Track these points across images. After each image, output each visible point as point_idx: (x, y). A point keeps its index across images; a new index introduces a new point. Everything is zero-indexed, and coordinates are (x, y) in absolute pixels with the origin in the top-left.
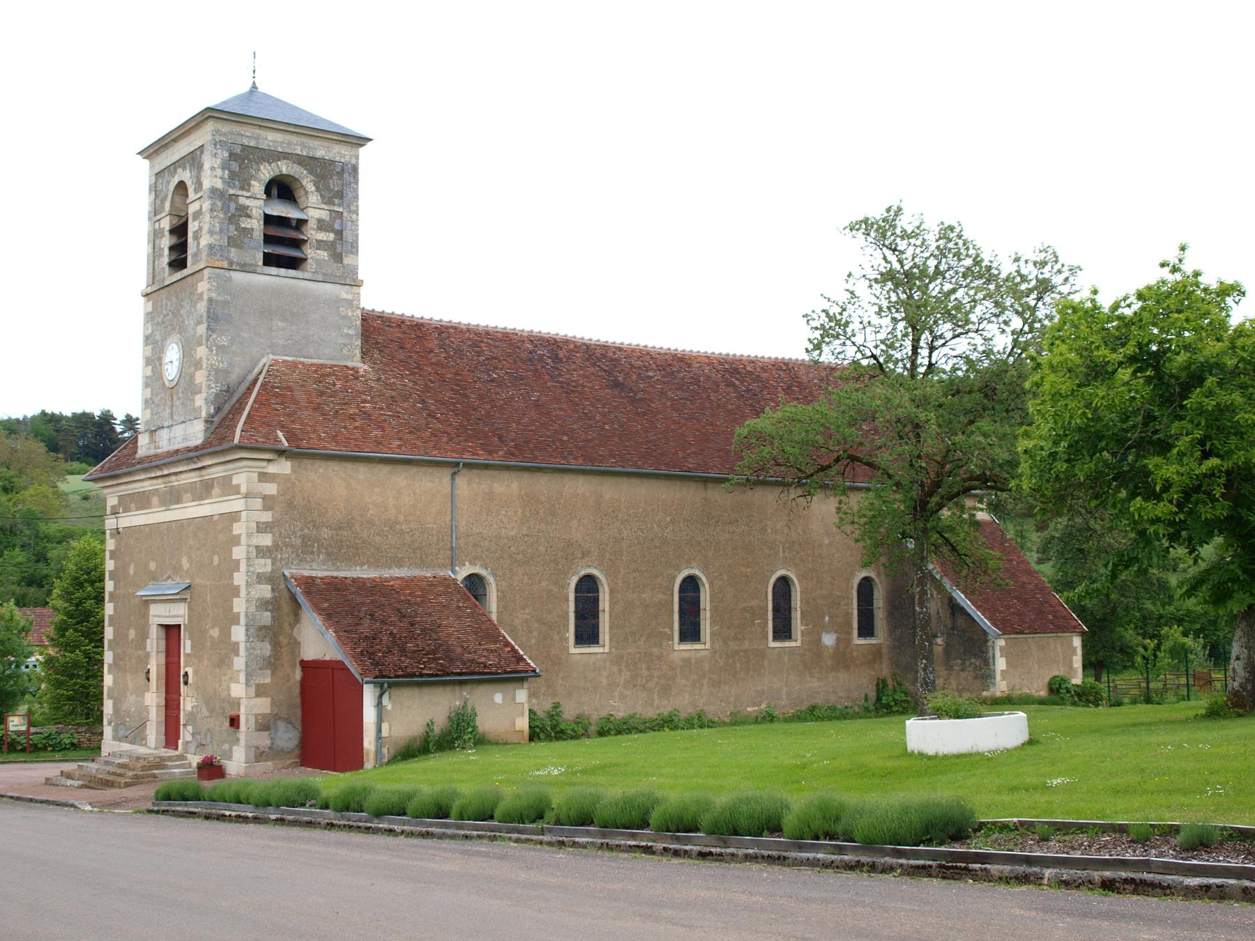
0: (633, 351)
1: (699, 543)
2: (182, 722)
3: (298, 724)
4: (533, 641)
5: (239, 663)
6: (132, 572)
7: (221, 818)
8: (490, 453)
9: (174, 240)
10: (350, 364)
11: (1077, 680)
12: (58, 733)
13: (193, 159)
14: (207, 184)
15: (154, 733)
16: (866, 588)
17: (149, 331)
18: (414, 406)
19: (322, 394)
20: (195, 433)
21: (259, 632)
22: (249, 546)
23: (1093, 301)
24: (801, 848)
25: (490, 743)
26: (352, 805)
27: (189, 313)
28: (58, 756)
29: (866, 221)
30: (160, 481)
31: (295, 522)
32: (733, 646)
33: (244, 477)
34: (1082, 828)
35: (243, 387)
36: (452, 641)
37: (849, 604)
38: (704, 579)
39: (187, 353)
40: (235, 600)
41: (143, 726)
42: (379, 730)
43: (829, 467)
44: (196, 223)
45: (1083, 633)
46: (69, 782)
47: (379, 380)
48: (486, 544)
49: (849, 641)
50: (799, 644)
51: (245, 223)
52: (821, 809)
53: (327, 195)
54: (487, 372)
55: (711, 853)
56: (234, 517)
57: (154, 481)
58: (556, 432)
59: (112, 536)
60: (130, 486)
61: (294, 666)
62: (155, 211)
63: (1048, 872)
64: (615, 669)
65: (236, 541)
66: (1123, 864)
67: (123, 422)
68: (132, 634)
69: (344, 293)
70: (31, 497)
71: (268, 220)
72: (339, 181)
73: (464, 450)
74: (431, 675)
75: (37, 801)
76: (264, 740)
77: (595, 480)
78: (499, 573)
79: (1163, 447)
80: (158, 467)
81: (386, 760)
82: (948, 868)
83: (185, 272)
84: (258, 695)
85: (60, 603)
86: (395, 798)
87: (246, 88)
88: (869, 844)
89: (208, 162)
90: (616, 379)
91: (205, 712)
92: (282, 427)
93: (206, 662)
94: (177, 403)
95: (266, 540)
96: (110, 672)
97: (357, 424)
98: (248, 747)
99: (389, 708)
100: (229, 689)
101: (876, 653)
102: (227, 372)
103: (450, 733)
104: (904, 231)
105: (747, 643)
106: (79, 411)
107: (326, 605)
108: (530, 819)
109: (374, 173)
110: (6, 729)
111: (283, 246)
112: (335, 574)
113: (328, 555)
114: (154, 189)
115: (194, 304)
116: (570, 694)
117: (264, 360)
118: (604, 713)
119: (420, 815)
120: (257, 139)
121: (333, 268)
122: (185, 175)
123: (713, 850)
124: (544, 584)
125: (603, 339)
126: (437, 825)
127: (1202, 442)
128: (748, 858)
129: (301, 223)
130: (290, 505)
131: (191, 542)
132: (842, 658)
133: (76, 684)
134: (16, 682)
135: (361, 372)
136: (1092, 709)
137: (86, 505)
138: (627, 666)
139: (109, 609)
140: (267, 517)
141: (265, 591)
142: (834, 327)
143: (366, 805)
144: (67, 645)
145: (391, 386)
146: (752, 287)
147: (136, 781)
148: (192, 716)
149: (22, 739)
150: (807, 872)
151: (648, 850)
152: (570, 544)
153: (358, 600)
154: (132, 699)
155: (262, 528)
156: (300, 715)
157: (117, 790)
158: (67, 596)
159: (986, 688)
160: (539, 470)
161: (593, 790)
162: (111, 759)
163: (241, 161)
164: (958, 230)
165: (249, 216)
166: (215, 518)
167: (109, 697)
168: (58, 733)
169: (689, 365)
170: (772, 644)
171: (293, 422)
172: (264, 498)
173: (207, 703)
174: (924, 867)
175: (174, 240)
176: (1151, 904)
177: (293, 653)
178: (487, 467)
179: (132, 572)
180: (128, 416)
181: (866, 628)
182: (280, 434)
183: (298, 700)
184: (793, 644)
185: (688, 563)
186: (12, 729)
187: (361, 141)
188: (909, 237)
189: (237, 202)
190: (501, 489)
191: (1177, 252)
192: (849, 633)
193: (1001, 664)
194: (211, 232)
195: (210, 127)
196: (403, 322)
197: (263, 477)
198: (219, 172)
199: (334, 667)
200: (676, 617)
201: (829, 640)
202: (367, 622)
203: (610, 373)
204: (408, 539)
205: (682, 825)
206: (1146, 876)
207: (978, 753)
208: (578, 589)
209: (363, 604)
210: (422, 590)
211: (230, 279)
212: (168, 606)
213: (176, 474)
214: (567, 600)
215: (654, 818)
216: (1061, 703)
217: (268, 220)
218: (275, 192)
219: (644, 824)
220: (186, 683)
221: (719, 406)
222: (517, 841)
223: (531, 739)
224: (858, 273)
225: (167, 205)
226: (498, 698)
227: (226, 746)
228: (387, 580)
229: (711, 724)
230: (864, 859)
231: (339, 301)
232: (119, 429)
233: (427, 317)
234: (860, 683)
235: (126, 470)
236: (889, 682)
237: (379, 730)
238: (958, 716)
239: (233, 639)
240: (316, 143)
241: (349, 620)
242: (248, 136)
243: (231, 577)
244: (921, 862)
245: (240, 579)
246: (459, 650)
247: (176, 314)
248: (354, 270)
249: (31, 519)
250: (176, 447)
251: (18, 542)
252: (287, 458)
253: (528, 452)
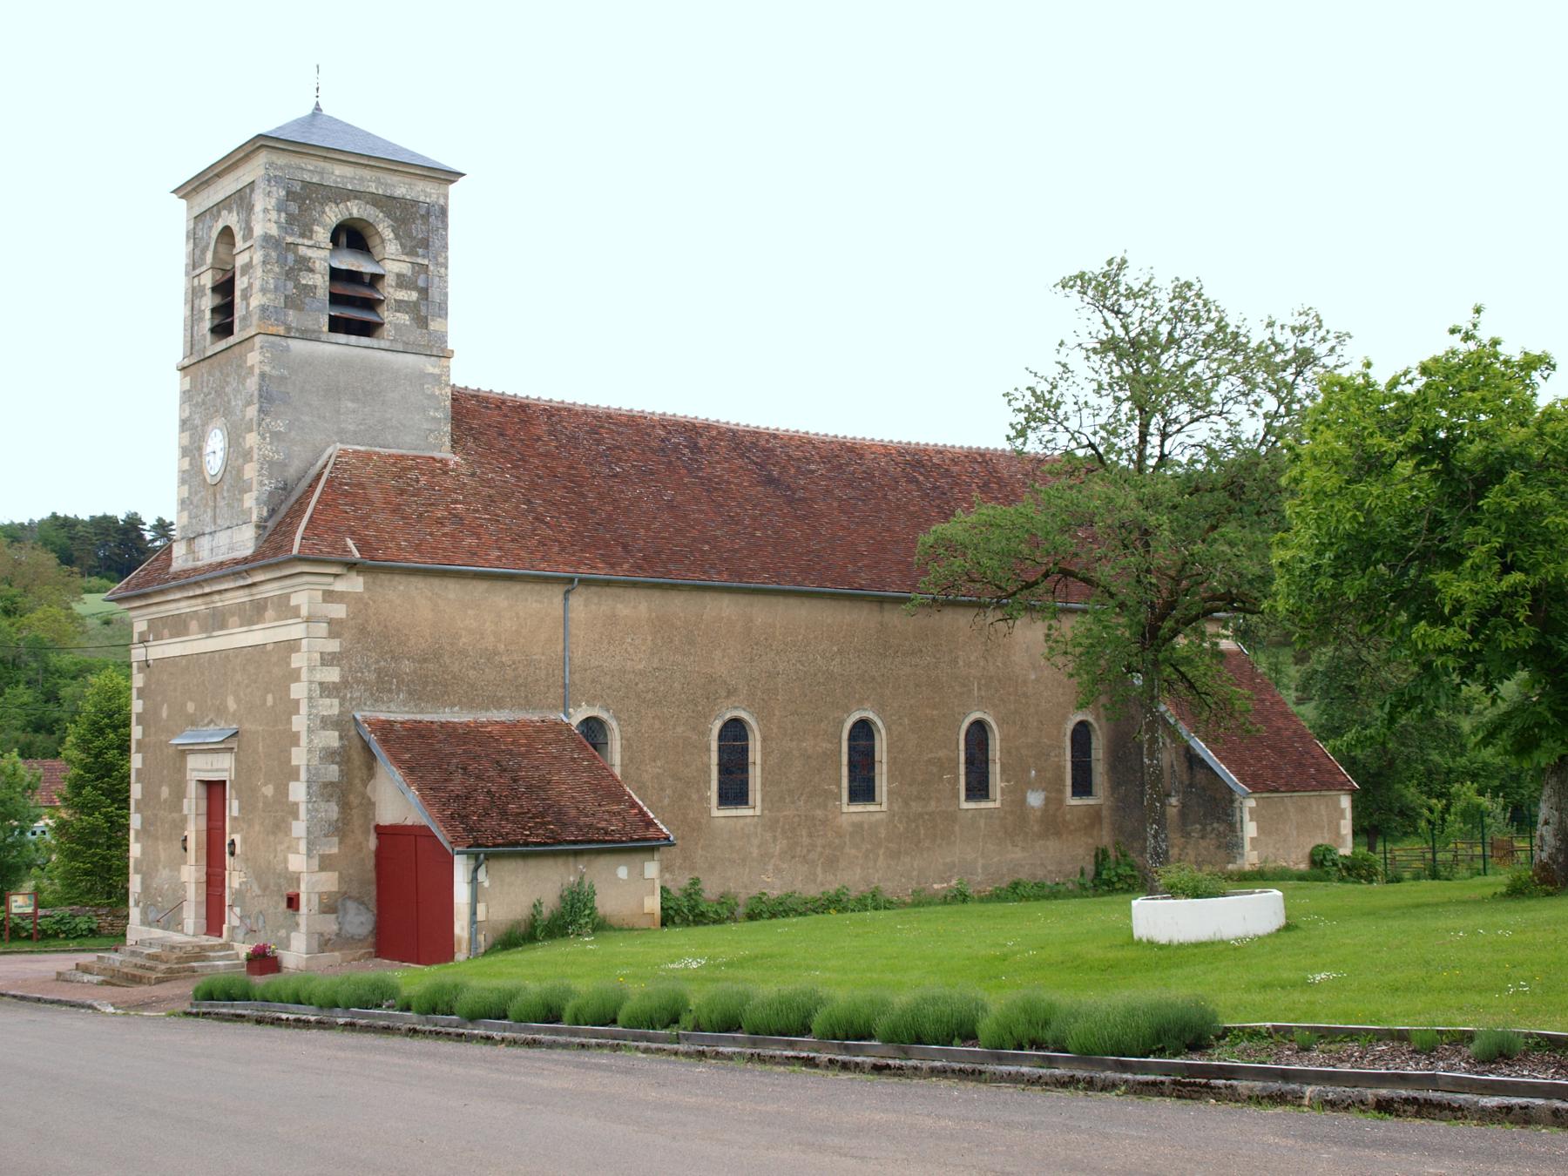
0: (791, 438)
1: (873, 679)
2: (227, 902)
3: (373, 905)
4: (666, 801)
5: (299, 828)
6: (164, 715)
7: (276, 1022)
8: (612, 566)
9: (218, 300)
10: (437, 455)
11: (1346, 850)
12: (73, 916)
13: (241, 198)
14: (258, 230)
15: (192, 916)
16: (1082, 734)
17: (187, 414)
18: (517, 507)
19: (402, 492)
20: (244, 541)
21: (324, 790)
22: (311, 682)
23: (1365, 376)
24: (1000, 1059)
25: (612, 928)
26: (440, 1007)
27: (236, 391)
28: (72, 945)
29: (1082, 276)
30: (200, 601)
31: (369, 652)
32: (916, 807)
33: (304, 596)
34: (1352, 1035)
35: (304, 484)
36: (565, 801)
37: (1061, 755)
38: (879, 723)
39: (234, 441)
40: (294, 750)
41: (179, 907)
42: (474, 913)
43: (1036, 583)
44: (245, 279)
45: (1353, 792)
46: (87, 978)
47: (473, 475)
48: (608, 679)
49: (1061, 801)
50: (998, 804)
51: (306, 279)
52: (1026, 1011)
53: (409, 244)
54: (608, 464)
55: (888, 1067)
56: (292, 646)
57: (193, 602)
58: (694, 540)
59: (140, 670)
60: (163, 608)
61: (367, 832)
62: (194, 264)
63: (1309, 1090)
64: (768, 836)
65: (295, 676)
66: (1404, 1079)
67: (154, 528)
68: (165, 792)
69: (430, 366)
70: (38, 621)
71: (335, 274)
72: (423, 226)
73: (580, 563)
74: (539, 844)
75: (46, 1001)
76: (330, 925)
77: (744, 600)
78: (624, 716)
79: (1453, 559)
80: (198, 584)
81: (482, 950)
82: (1185, 1085)
83: (231, 340)
84: (322, 868)
85: (75, 754)
86: (493, 998)
87: (308, 110)
88: (1086, 1055)
89: (260, 202)
90: (770, 474)
91: (256, 890)
92: (352, 534)
93: (257, 828)
94: (221, 503)
95: (333, 675)
96: (137, 840)
97: (446, 530)
98: (310, 934)
99: (486, 884)
100: (286, 861)
101: (1095, 816)
102: (283, 465)
103: (562, 916)
104: (1129, 288)
105: (933, 803)
106: (99, 514)
107: (407, 756)
108: (663, 1024)
109: (467, 216)
110: (8, 911)
111: (354, 307)
112: (419, 717)
113: (410, 693)
114: (193, 236)
115: (242, 380)
116: (712, 868)
117: (329, 451)
118: (755, 892)
119: (525, 1018)
120: (321, 173)
121: (416, 335)
122: (231, 219)
123: (890, 1062)
124: (679, 730)
126: (546, 1031)
127: (1501, 553)
128: (934, 1072)
129: (376, 279)
130: (363, 631)
131: (238, 677)
132: (1052, 823)
133: (94, 855)
134: (20, 853)
135: (451, 465)
136: (1364, 886)
137: (108, 630)
138: (784, 832)
139: (136, 761)
140: (334, 646)
141: (332, 739)
142: (1042, 409)
143: (457, 1006)
144: (84, 806)
145: (488, 483)
146: (940, 358)
147: (170, 976)
148: (240, 895)
149: (28, 924)
150: (1008, 1090)
151: (810, 1062)
152: (712, 680)
153: (448, 749)
154: (165, 873)
155: (328, 660)
156: (374, 893)
157: (146, 988)
158: (83, 745)
159: (1232, 860)
160: (674, 587)
161: (741, 987)
162: (139, 949)
163: (301, 201)
165: (312, 271)
166: (269, 648)
167: (137, 872)
168: (73, 916)
169: (861, 457)
170: (965, 805)
171: (366, 527)
172: (330, 622)
173: (258, 878)
174: (1154, 1084)
175: (218, 300)
176: (1438, 1130)
177: (366, 816)
178: (608, 583)
179: (164, 715)
180: (160, 520)
181: (1082, 785)
182: (350, 542)
183: (372, 875)
184: (991, 805)
185: (860, 704)
186: (14, 910)
187: (451, 176)
188: (1136, 296)
189: (296, 253)
190: (626, 612)
191: (1470, 314)
192: (1061, 791)
193: (1250, 829)
194: (264, 290)
196: (503, 402)
197: (329, 596)
198: (274, 215)
200: (845, 771)
201: (1035, 799)
202: (458, 777)
203: (762, 466)
204: (510, 673)
205: (852, 1032)
206: (1432, 1095)
207: (1222, 942)
208: (722, 736)
209: (453, 755)
210: (528, 737)
211: (287, 349)
212: (210, 757)
213: (220, 592)
214: (709, 750)
215: (817, 1022)
216: (1326, 878)
217: (335, 274)
218: (343, 240)
219: (805, 1030)
220: (232, 854)
221: (898, 508)
222: (646, 1050)
223: (663, 924)
224: (1072, 342)
225: (209, 256)
226: (623, 872)
227: (282, 933)
228: (483, 725)
229: (889, 905)
230: (1079, 1073)
231: (424, 376)
232: (148, 536)
233: (534, 396)
234: (1075, 854)
235: (157, 588)
236: (1111, 852)
237: (474, 913)
238: (1197, 894)
239: (292, 798)
240: (395, 179)
241: (436, 775)
242: (310, 170)
243: (289, 722)
244: (1151, 1078)
245: (299, 723)
246: (573, 812)
247: (220, 393)
248: (442, 338)
249: (38, 649)
250: (220, 558)
251: (23, 678)
252: (359, 572)
253: (659, 565)
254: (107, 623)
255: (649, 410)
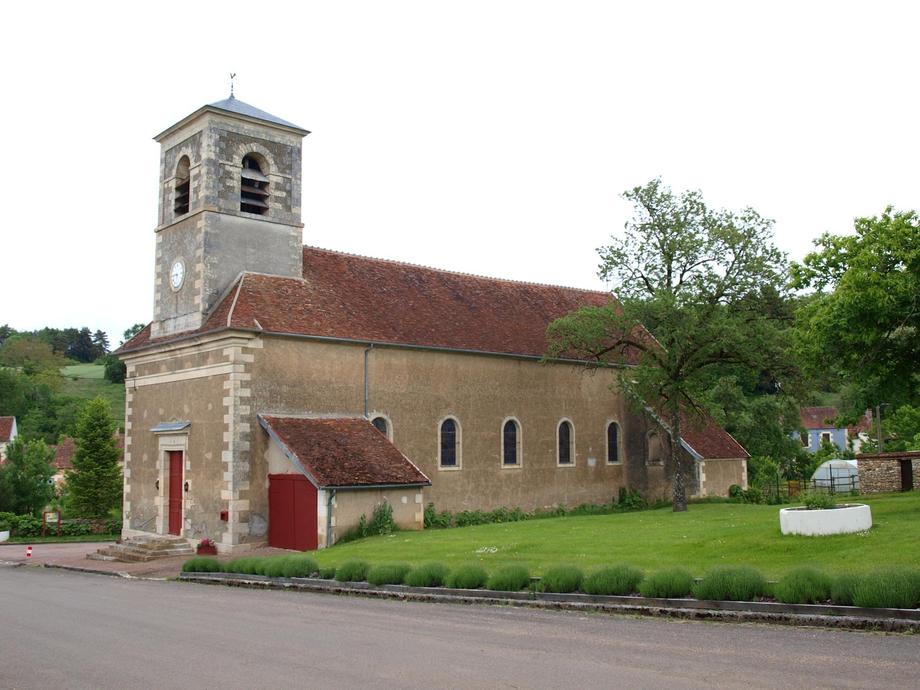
0: (466, 277)
1: (516, 400)
2: (183, 516)
3: (267, 518)
5: (228, 476)
6: (145, 415)
7: (240, 585)
8: (389, 338)
9: (178, 195)
10: (296, 278)
11: (745, 488)
12: (78, 524)
13: (194, 140)
14: (204, 156)
15: (161, 524)
16: (613, 429)
17: (160, 255)
18: (338, 307)
19: (280, 297)
20: (195, 321)
22: (235, 397)
24: (796, 610)
26: (353, 577)
27: (191, 242)
28: (78, 539)
29: (637, 190)
30: (167, 354)
31: (264, 379)
32: (536, 466)
33: (231, 350)
35: (227, 292)
37: (603, 440)
38: (519, 423)
42: (329, 522)
43: (613, 348)
44: (196, 182)
46: (105, 558)
47: (315, 289)
49: (603, 463)
51: (229, 183)
52: (809, 579)
53: (282, 167)
54: (380, 287)
55: (709, 615)
56: (225, 377)
57: (164, 355)
58: (427, 326)
59: (131, 392)
60: (145, 358)
61: (264, 478)
62: (165, 176)
64: (466, 481)
65: (226, 393)
67: (96, 335)
68: (145, 457)
69: (292, 232)
71: (245, 182)
72: (289, 158)
73: (373, 336)
74: (381, 484)
75: (87, 571)
76: (245, 529)
77: (454, 357)
78: (395, 417)
80: (167, 345)
81: (334, 542)
83: (187, 215)
84: (241, 498)
87: (227, 97)
88: (869, 607)
89: (205, 141)
91: (201, 509)
92: (257, 317)
95: (247, 393)
96: (128, 483)
97: (304, 317)
98: (234, 534)
99: (336, 506)
100: (220, 494)
101: (619, 470)
103: (375, 524)
104: (663, 196)
106: (69, 328)
107: (288, 437)
108: (432, 584)
109: (311, 152)
110: (45, 521)
111: (254, 199)
112: (291, 416)
113: (286, 403)
114: (165, 161)
115: (194, 236)
117: (241, 274)
119: (418, 583)
120: (238, 128)
121: (285, 215)
122: (188, 151)
123: (710, 612)
125: (447, 270)
126: (433, 592)
128: (747, 618)
129: (263, 185)
130: (263, 369)
131: (191, 394)
132: (600, 474)
133: (89, 492)
134: (44, 491)
136: (755, 505)
137: (76, 383)
140: (247, 377)
141: (246, 427)
142: (614, 259)
143: (368, 576)
144: (84, 466)
145: (322, 294)
147: (155, 557)
148: (191, 513)
149: (55, 528)
150: (800, 630)
155: (244, 384)
156: (268, 511)
157: (142, 563)
160: (419, 350)
161: (362, 561)
162: (135, 542)
163: (227, 141)
164: (698, 194)
165: (232, 179)
166: (210, 378)
167: (127, 500)
168: (78, 524)
169: (500, 288)
170: (559, 465)
171: (264, 314)
172: (246, 364)
175: (178, 195)
177: (264, 469)
179: (145, 415)
180: (99, 331)
181: (613, 456)
183: (267, 502)
184: (571, 465)
186: (48, 521)
187: (303, 133)
189: (224, 169)
192: (604, 458)
193: (703, 477)
194: (207, 188)
195: (203, 124)
196: (325, 253)
197: (245, 350)
198: (213, 148)
199: (301, 479)
200: (502, 447)
209: (312, 436)
210: (349, 428)
211: (219, 219)
212: (173, 438)
213: (180, 349)
214: (437, 435)
215: (408, 577)
216: (738, 501)
217: (245, 182)
218: (247, 164)
219: (400, 582)
220: (186, 490)
221: (521, 313)
222: (516, 604)
223: (425, 528)
225: (174, 172)
226: (405, 500)
227: (218, 533)
228: (325, 421)
230: (869, 619)
231: (289, 236)
232: (93, 339)
233: (340, 251)
234: (606, 491)
235: (143, 347)
236: (627, 489)
237: (329, 522)
242: (232, 126)
243: (222, 418)
245: (229, 419)
246: (378, 467)
248: (298, 217)
249: (45, 391)
250: (180, 331)
251: (37, 405)
252: (261, 338)
254: (76, 379)
255: (397, 260)
